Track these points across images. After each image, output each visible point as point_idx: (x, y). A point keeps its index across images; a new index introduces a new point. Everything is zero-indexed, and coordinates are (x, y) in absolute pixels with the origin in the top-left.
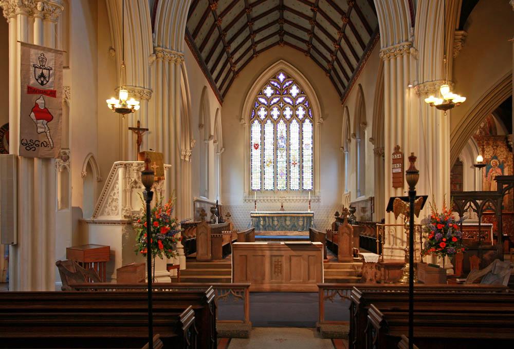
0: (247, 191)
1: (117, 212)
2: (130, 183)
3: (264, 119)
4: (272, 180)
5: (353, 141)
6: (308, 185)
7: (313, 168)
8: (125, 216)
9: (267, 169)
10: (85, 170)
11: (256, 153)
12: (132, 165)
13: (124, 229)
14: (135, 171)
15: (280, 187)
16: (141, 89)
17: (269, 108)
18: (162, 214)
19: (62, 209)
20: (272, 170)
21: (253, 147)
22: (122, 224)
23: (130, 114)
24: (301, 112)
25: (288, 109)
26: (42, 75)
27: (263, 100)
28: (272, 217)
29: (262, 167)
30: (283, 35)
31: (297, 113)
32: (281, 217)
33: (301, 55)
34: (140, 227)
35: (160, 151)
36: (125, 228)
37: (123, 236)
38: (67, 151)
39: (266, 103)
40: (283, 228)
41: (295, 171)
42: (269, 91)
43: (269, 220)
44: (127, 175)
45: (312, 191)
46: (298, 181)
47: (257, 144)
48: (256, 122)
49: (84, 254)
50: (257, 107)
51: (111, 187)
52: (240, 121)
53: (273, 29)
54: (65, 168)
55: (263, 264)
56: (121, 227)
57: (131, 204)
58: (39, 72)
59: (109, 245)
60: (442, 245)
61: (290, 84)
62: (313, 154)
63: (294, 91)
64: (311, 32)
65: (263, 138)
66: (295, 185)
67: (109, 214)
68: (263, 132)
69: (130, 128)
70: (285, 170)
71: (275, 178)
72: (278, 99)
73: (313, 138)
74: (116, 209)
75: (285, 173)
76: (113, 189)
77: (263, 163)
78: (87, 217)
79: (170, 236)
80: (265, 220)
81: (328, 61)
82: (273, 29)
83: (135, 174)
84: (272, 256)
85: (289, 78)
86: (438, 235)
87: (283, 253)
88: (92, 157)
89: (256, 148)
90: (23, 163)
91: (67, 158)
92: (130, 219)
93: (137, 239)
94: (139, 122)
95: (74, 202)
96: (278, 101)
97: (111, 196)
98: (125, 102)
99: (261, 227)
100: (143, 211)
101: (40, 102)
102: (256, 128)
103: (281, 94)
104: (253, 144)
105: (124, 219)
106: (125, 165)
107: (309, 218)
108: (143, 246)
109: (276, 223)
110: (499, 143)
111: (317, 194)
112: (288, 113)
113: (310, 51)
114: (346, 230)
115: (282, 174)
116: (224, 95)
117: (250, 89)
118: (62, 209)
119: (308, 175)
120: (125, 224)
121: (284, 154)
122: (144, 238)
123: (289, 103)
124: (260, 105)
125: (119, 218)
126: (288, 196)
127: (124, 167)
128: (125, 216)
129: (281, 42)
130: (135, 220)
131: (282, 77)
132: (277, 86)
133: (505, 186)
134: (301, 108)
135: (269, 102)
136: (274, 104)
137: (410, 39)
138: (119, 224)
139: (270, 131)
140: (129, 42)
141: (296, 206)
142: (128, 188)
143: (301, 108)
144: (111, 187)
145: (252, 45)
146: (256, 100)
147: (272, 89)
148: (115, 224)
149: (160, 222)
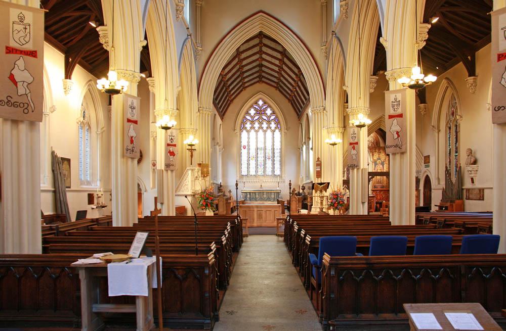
0: (239, 176)
5: (304, 146)
6: (277, 172)
7: (281, 161)
11: (244, 152)
15: (259, 173)
16: (132, 72)
17: (252, 122)
18: (209, 191)
23: (170, 130)
24: (273, 125)
25: (265, 123)
26: (172, 139)
27: (248, 117)
28: (255, 193)
29: (248, 160)
30: (262, 54)
33: (274, 89)
35: (207, 163)
40: (262, 199)
41: (269, 163)
42: (252, 112)
45: (280, 176)
48: (244, 131)
53: (256, 49)
55: (253, 215)
58: (171, 138)
60: (336, 205)
61: (266, 108)
62: (281, 152)
63: (269, 112)
64: (281, 68)
66: (269, 171)
71: (257, 167)
73: (281, 142)
76: (185, 180)
77: (249, 158)
80: (250, 195)
81: (293, 86)
82: (256, 49)
84: (258, 211)
85: (265, 103)
86: (334, 201)
87: (263, 209)
89: (244, 148)
90: (165, 172)
98: (115, 83)
99: (248, 199)
101: (171, 149)
102: (244, 134)
104: (242, 146)
107: (278, 193)
109: (257, 196)
110: (381, 151)
111: (283, 178)
112: (265, 125)
113: (279, 87)
114: (294, 199)
116: (224, 115)
119: (277, 165)
121: (263, 152)
123: (265, 120)
126: (264, 179)
129: (260, 81)
131: (261, 103)
133: (370, 177)
134: (273, 123)
136: (256, 120)
137: (324, 106)
140: (121, 33)
141: (269, 184)
143: (273, 123)
145: (239, 68)
147: (255, 110)
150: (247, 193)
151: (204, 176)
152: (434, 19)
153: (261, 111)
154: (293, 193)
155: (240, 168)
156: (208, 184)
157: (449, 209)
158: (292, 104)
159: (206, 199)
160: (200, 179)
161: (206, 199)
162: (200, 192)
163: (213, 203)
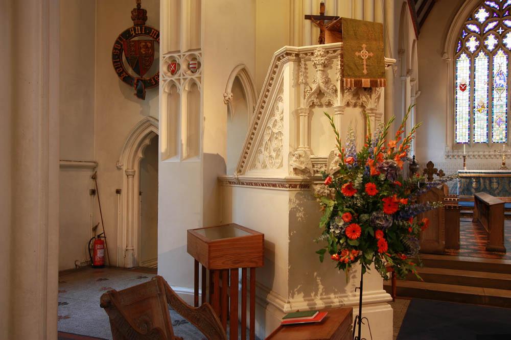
0: (450, 144)
1: (279, 161)
2: (308, 95)
3: (474, 51)
4: (486, 129)
8: (295, 169)
9: (477, 115)
10: (229, 90)
11: (462, 97)
12: (312, 54)
13: (293, 198)
14: (320, 67)
19: (189, 156)
20: (486, 117)
21: (458, 88)
22: (290, 186)
27: (473, 28)
28: (490, 179)
29: (472, 113)
32: (503, 178)
34: (329, 197)
35: (380, 20)
36: (296, 196)
37: (292, 214)
38: (196, 53)
39: (477, 30)
42: (482, 15)
43: (484, 182)
44: (301, 78)
47: (463, 85)
48: (463, 56)
49: (210, 251)
50: (465, 36)
51: (268, 112)
52: (442, 57)
54: (194, 84)
56: (288, 193)
57: (309, 144)
59: (263, 232)
65: (472, 77)
67: (265, 167)
68: (472, 69)
69: (307, 17)
70: (505, 115)
71: (490, 127)
72: (495, 23)
74: (278, 155)
75: (505, 119)
76: (272, 114)
77: (472, 108)
78: (231, 174)
79: (403, 218)
83: (319, 74)
88: (244, 70)
89: (463, 90)
91: (196, 66)
92: (306, 177)
93: (322, 225)
94: (322, 5)
95: (209, 145)
96: (495, 27)
97: (269, 128)
100: (337, 158)
102: (463, 63)
103: (501, 16)
104: (458, 85)
105: (293, 176)
106: (297, 55)
108: (338, 242)
109: (495, 185)
115: (501, 120)
117: (452, 22)
118: (189, 156)
120: (295, 186)
122: (341, 224)
124: (468, 34)
125: (284, 173)
127: (294, 61)
128: (295, 169)
130: (319, 179)
132: (493, 7)
135: (482, 29)
136: (490, 30)
138: (283, 186)
139: (483, 67)
142: (302, 106)
144: (268, 112)
146: (464, 28)
147: (487, 11)
148: (274, 185)
149: (379, 184)
150: (470, 178)
151: (358, 84)
155: (454, 129)
156: (375, 130)
159: (366, 209)
160: (338, 101)
161: (366, 209)
162: (334, 167)
163: (404, 230)
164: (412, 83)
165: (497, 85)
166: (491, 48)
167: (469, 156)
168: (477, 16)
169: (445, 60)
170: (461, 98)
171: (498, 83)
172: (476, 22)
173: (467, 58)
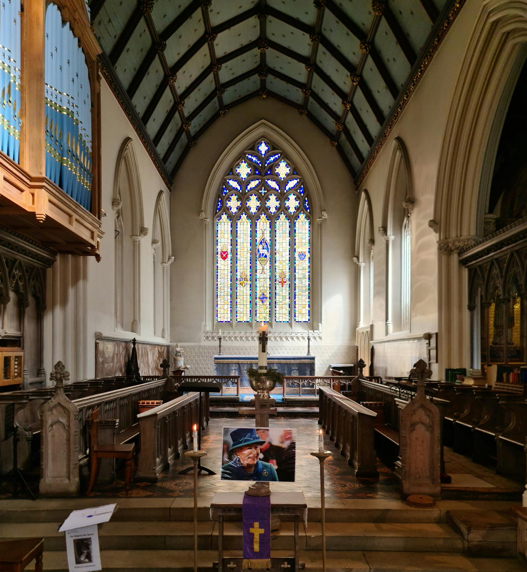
11: (224, 266)
17: (243, 197)
24: (292, 203)
27: (234, 184)
29: (233, 288)
31: (287, 203)
41: (283, 292)
42: (244, 170)
46: (288, 308)
47: (224, 253)
61: (276, 160)
63: (283, 170)
65: (234, 243)
68: (234, 233)
72: (295, 182)
77: (233, 279)
85: (274, 149)
89: (224, 258)
96: (257, 186)
112: (273, 203)
131: (263, 148)
134: (292, 197)
143: (292, 197)
146: (224, 182)
152: (403, 383)
153: (263, 167)
154: (208, 450)
157: (446, 240)
158: (340, 150)
164: (154, 246)
165: (260, 254)
166: (253, 210)
167: (224, 337)
168: (238, 170)
169: (202, 220)
170: (222, 268)
171: (261, 253)
172: (237, 178)
173: (228, 221)
